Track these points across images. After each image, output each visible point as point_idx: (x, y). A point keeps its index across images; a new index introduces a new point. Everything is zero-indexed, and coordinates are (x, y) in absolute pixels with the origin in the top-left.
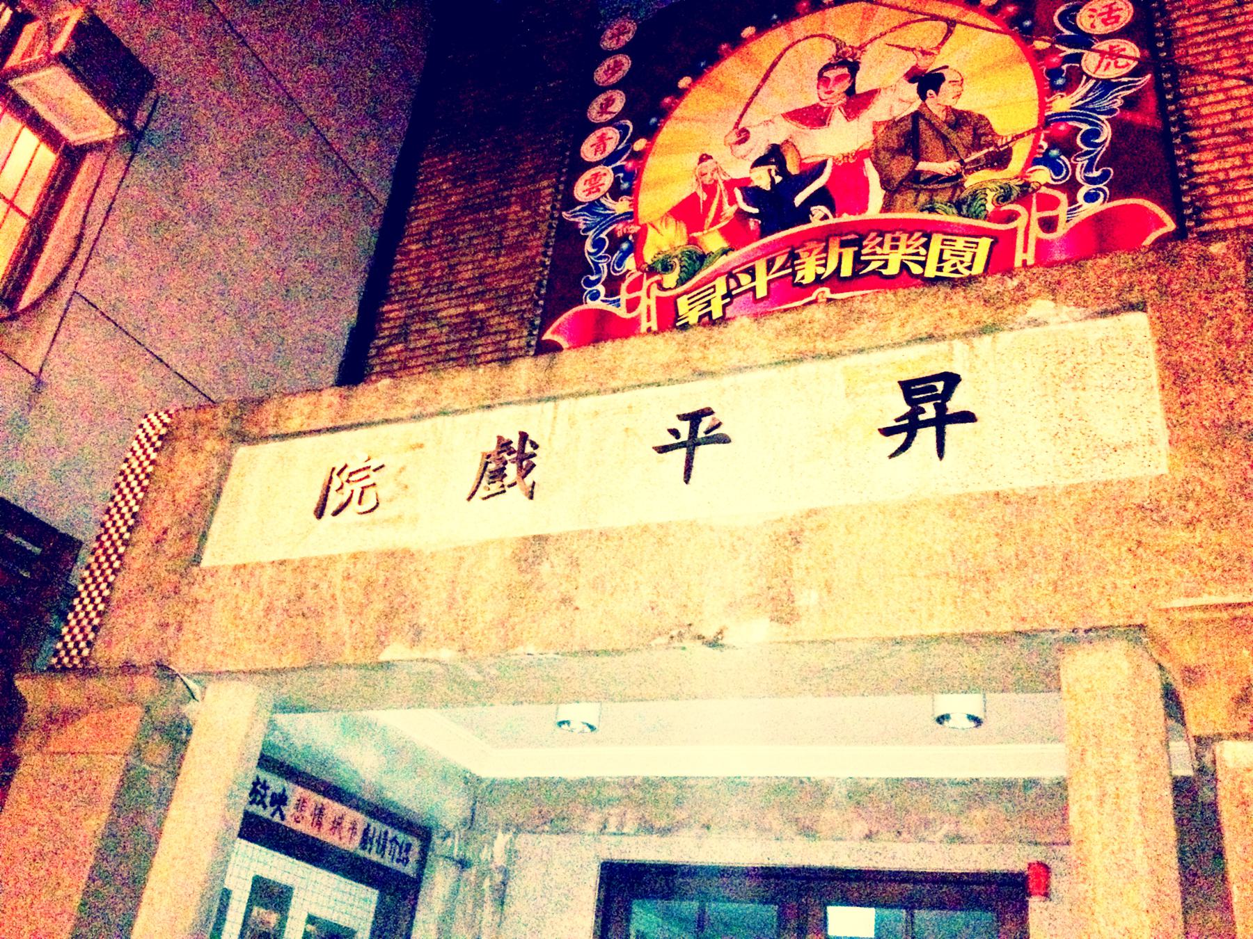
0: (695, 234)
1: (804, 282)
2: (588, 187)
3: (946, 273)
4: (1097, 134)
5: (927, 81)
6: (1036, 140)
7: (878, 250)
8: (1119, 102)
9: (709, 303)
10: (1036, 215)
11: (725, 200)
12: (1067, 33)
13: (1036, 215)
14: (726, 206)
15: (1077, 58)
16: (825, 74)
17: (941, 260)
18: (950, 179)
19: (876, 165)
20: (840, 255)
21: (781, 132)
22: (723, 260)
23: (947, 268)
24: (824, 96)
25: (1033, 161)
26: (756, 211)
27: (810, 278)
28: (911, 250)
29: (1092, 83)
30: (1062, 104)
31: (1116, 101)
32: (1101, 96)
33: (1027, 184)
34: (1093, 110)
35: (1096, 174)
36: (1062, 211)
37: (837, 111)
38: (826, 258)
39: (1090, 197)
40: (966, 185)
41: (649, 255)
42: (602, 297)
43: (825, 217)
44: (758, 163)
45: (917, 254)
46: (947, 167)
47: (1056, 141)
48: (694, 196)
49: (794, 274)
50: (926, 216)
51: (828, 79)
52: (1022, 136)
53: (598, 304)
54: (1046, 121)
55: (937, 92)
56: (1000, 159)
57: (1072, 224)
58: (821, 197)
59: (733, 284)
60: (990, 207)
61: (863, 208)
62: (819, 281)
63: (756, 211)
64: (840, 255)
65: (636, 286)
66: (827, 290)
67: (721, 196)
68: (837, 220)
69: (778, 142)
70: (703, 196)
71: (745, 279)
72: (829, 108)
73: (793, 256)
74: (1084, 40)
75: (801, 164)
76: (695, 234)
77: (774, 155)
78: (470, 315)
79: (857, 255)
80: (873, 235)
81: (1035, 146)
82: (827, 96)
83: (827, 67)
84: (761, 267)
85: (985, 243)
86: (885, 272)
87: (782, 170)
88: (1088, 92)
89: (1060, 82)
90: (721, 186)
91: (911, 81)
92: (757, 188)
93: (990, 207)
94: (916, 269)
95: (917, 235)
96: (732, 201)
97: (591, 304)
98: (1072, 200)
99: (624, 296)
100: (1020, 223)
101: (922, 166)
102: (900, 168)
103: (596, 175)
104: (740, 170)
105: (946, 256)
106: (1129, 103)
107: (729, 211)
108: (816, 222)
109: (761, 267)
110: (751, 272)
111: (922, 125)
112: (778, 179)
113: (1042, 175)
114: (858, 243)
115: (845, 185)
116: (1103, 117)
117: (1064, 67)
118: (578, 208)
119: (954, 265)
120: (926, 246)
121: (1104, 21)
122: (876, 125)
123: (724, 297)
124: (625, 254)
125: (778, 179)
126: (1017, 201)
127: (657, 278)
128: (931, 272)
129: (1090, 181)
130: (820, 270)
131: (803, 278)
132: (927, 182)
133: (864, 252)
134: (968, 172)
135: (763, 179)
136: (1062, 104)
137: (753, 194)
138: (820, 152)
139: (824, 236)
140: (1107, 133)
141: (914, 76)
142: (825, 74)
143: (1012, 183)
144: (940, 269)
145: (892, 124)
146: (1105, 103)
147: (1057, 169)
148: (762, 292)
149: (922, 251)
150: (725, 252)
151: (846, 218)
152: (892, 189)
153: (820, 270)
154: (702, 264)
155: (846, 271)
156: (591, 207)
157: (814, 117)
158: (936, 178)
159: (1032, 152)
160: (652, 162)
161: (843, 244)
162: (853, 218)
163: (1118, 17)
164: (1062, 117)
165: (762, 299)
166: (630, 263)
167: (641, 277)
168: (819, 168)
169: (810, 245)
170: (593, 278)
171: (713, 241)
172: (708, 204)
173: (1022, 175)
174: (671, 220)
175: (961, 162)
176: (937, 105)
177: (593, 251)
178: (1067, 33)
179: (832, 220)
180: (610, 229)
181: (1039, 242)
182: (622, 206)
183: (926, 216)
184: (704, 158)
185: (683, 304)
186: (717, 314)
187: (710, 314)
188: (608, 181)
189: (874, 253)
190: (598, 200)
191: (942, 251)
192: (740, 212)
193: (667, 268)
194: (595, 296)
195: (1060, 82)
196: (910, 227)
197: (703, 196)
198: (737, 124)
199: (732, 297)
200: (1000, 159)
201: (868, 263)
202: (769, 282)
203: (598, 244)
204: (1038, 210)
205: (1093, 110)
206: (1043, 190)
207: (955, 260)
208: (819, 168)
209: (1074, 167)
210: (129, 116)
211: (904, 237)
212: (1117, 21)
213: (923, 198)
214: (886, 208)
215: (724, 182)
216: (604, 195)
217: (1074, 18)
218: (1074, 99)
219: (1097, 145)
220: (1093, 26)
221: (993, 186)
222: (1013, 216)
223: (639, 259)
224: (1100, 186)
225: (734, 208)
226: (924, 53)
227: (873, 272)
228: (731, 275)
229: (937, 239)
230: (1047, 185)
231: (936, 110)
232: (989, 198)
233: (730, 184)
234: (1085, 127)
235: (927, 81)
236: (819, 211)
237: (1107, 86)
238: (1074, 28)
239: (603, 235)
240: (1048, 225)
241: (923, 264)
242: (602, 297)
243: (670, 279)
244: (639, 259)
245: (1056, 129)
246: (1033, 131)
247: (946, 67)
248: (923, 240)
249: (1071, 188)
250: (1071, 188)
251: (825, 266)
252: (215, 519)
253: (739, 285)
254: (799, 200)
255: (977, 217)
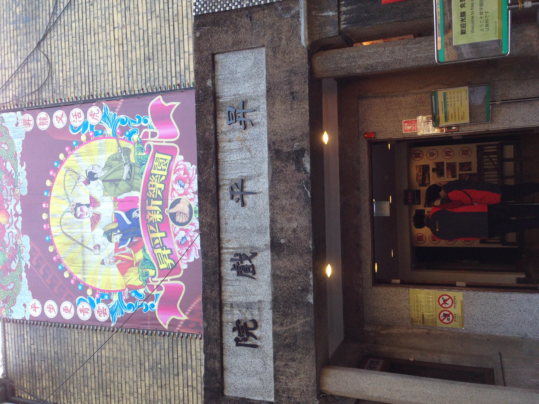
0: (135, 264)
1: (162, 218)
2: (102, 315)
3: (166, 168)
4: (123, 120)
5: (91, 177)
6: (121, 139)
7: (154, 191)
8: (112, 112)
9: (164, 255)
10: (150, 139)
11: (123, 252)
12: (81, 129)
13: (150, 139)
14: (125, 252)
15: (92, 126)
16: (78, 216)
17: (161, 170)
18: (131, 168)
19: (120, 194)
20: (153, 205)
21: (99, 231)
22: (148, 251)
23: (164, 167)
24: (88, 216)
25: (129, 141)
26: (130, 239)
27: (161, 216)
28: (156, 180)
29: (102, 121)
30: (109, 131)
31: (111, 113)
32: (108, 119)
33: (138, 142)
34: (113, 121)
35: (137, 120)
36: (149, 131)
37: (95, 210)
38: (154, 211)
39: (146, 121)
40: (134, 162)
41: (139, 283)
42: (154, 303)
43: (138, 212)
44: (110, 239)
45: (158, 178)
46: (126, 169)
47: (123, 132)
48: (118, 266)
49: (158, 222)
50: (144, 176)
51: (81, 215)
52: (119, 144)
53: (156, 304)
54: (115, 136)
55: (96, 174)
56: (127, 151)
57: (154, 127)
58: (129, 214)
59: (158, 246)
60: (144, 154)
61: (137, 198)
62: (162, 213)
63: (130, 239)
64: (153, 205)
65: (151, 288)
66: (166, 209)
67: (121, 254)
68: (140, 208)
69: (103, 232)
70: (119, 261)
71: (157, 241)
72: (94, 213)
73: (152, 224)
74: (85, 125)
75: (115, 222)
76: (135, 264)
77: (108, 235)
78: (151, 368)
79: (155, 199)
80: (148, 194)
81: (124, 139)
82: (88, 214)
83: (75, 215)
84: (153, 235)
85: (157, 155)
86: (163, 189)
87: (114, 230)
88: (106, 122)
89: (100, 132)
90: (117, 255)
91: (89, 183)
92: (121, 240)
93: (144, 154)
94: (163, 178)
95: (150, 178)
96: (124, 249)
97: (156, 308)
98: (146, 127)
99: (155, 293)
100: (152, 144)
101: (124, 178)
102: (123, 185)
103: (98, 312)
104: (111, 247)
105: (160, 168)
106: (113, 109)
107: (128, 250)
108: (139, 215)
109: (153, 235)
110: (154, 239)
111: (108, 178)
112: (119, 231)
113: (135, 137)
114: (150, 199)
115: (127, 205)
116: (116, 118)
117: (95, 130)
118: (111, 319)
119: (164, 165)
120: (155, 175)
121: (79, 117)
122: (104, 195)
123: (163, 249)
124: (137, 293)
125: (119, 231)
126: (144, 146)
127: (150, 279)
128: (165, 173)
129: (139, 122)
130: (158, 212)
131: (160, 219)
132: (130, 175)
133: (153, 197)
134: (129, 162)
135: (117, 238)
136: (109, 131)
137: (123, 241)
138: (111, 215)
139: (144, 212)
140: (122, 116)
141: (87, 182)
142: (78, 216)
143: (136, 147)
144: (164, 170)
145: (105, 190)
146: (111, 118)
147: (134, 132)
148: (163, 234)
149: (157, 176)
150: (145, 250)
151: (139, 204)
152: (132, 188)
153: (158, 212)
154: (148, 260)
155: (160, 203)
156: (112, 312)
157: (95, 219)
158: (130, 173)
159: (126, 140)
160: (98, 286)
161: (149, 204)
162: (140, 202)
163: (79, 113)
164: (114, 132)
165: (166, 234)
166: (141, 291)
167: (148, 286)
168: (118, 216)
169: (148, 217)
170: (144, 308)
171: (139, 256)
172: (123, 259)
173: (134, 144)
174: (126, 274)
175: (125, 164)
176: (100, 173)
177: (132, 309)
178: (81, 129)
179: (139, 210)
180: (124, 302)
181: (159, 138)
182: (115, 297)
183: (144, 176)
184: (103, 263)
185: (162, 266)
186: (169, 252)
187: (168, 255)
188: (102, 305)
189: (155, 193)
190: (109, 309)
191: (158, 170)
192: (129, 246)
193: (147, 274)
194: (153, 306)
195: (100, 132)
196: (147, 181)
197: (119, 261)
198: (91, 250)
199: (163, 245)
200: (127, 151)
201: (158, 195)
202: (160, 232)
203: (129, 307)
204: (151, 132)
205: (113, 121)
206: (141, 137)
207: (162, 165)
208: (118, 216)
209: (134, 127)
210: (146, 195)
211: (150, 183)
212: (80, 114)
213: (136, 177)
214: (138, 190)
215: (115, 252)
216: (108, 306)
217: (75, 128)
218: (108, 127)
219: (127, 119)
220: (80, 121)
221: (136, 154)
222: (149, 147)
223: (141, 287)
224: (142, 118)
225: (127, 248)
226: (78, 179)
227: (162, 193)
228: (154, 248)
229: (153, 171)
230: (139, 136)
231: (103, 174)
232: (141, 154)
233: (116, 250)
234: (119, 123)
235: (91, 177)
236: (134, 214)
237: (105, 116)
238: (80, 127)
239: (126, 305)
240: (154, 135)
241: (162, 176)
242: (154, 303)
243: (152, 272)
244: (141, 287)
245: (118, 134)
246: (117, 140)
247: (86, 171)
248: (153, 176)
249: (141, 128)
250: (141, 128)
251: (156, 211)
252: (268, 214)
253: (159, 243)
254: (129, 222)
255: (147, 158)
